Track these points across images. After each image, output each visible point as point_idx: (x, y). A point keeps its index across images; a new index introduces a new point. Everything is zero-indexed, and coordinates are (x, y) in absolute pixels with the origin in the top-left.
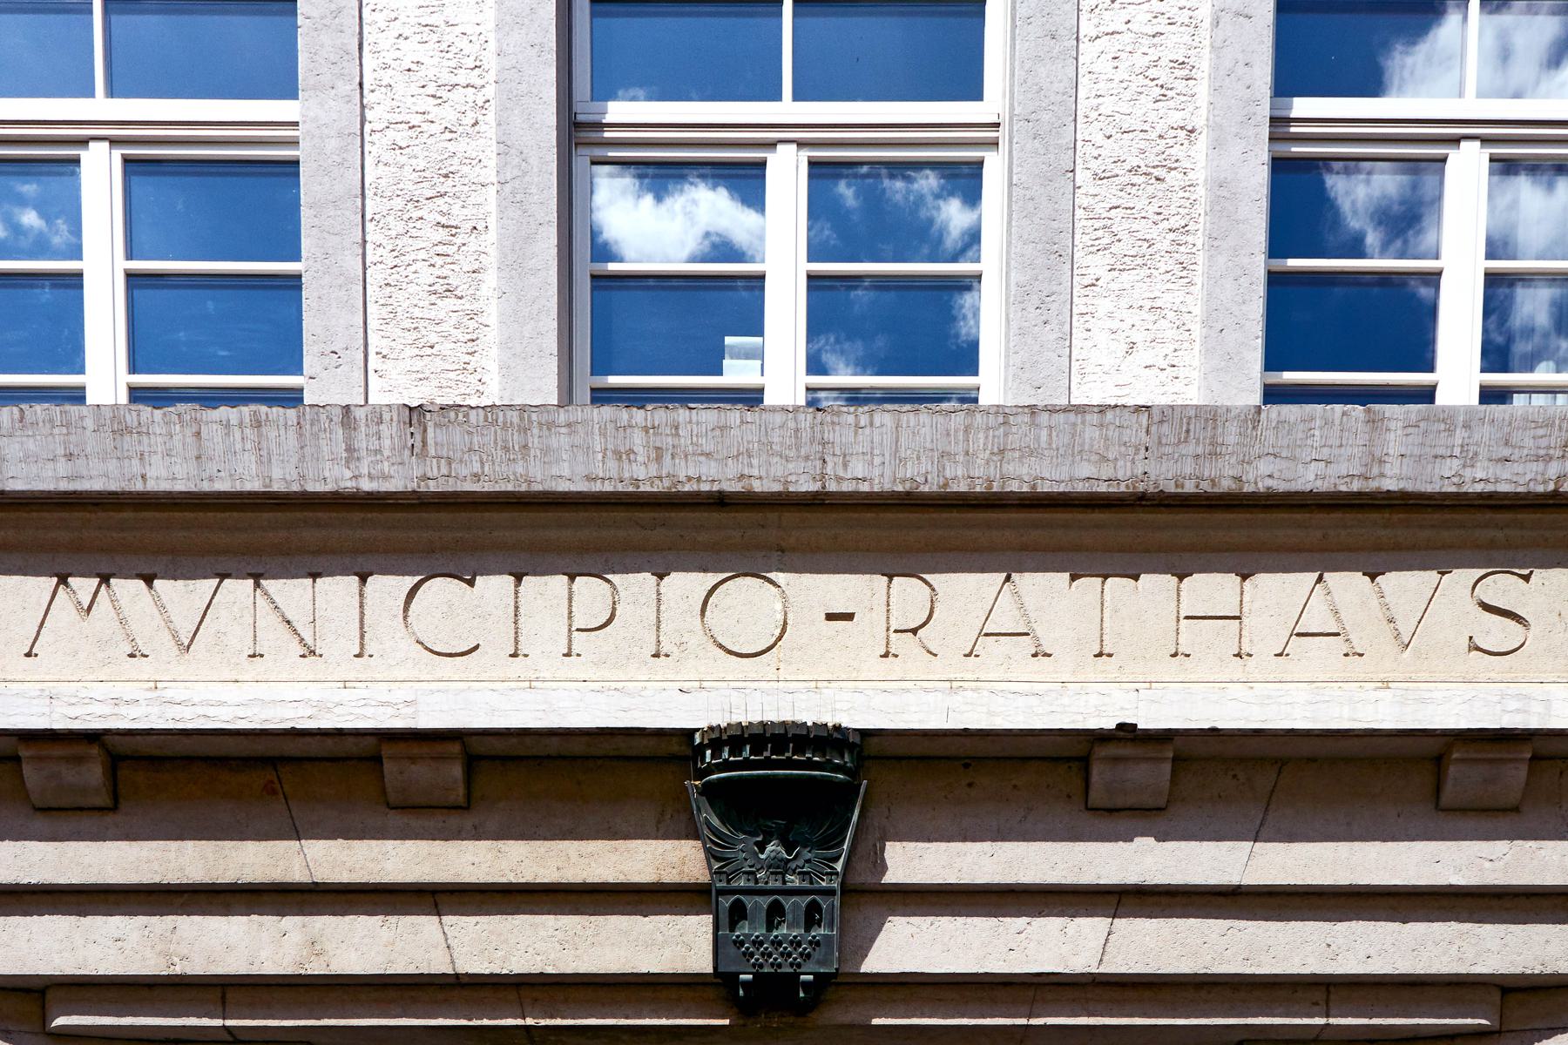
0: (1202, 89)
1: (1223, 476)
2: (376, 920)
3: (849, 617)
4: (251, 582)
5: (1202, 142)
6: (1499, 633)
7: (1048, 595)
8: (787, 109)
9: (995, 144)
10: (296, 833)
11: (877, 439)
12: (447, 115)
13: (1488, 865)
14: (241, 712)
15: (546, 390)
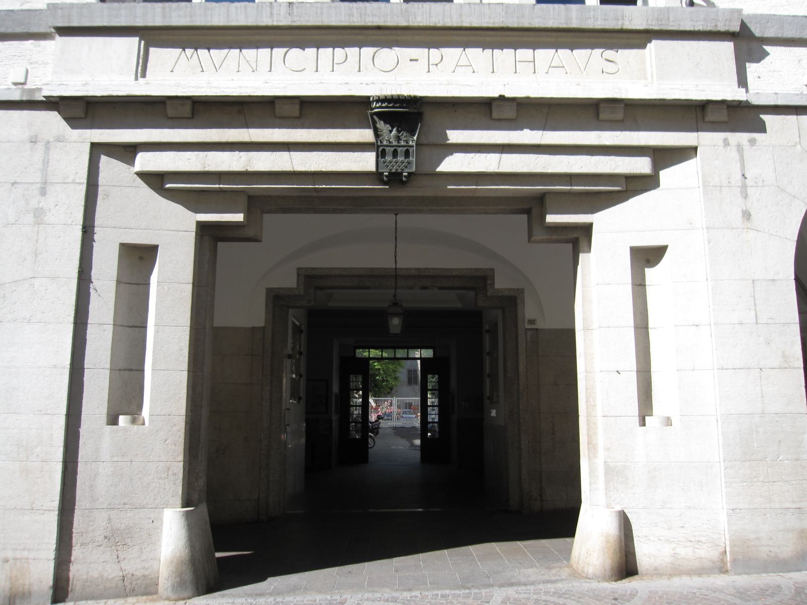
1: (526, 23)
2: (269, 153)
3: (417, 60)
6: (610, 67)
11: (424, 12)
13: (615, 138)
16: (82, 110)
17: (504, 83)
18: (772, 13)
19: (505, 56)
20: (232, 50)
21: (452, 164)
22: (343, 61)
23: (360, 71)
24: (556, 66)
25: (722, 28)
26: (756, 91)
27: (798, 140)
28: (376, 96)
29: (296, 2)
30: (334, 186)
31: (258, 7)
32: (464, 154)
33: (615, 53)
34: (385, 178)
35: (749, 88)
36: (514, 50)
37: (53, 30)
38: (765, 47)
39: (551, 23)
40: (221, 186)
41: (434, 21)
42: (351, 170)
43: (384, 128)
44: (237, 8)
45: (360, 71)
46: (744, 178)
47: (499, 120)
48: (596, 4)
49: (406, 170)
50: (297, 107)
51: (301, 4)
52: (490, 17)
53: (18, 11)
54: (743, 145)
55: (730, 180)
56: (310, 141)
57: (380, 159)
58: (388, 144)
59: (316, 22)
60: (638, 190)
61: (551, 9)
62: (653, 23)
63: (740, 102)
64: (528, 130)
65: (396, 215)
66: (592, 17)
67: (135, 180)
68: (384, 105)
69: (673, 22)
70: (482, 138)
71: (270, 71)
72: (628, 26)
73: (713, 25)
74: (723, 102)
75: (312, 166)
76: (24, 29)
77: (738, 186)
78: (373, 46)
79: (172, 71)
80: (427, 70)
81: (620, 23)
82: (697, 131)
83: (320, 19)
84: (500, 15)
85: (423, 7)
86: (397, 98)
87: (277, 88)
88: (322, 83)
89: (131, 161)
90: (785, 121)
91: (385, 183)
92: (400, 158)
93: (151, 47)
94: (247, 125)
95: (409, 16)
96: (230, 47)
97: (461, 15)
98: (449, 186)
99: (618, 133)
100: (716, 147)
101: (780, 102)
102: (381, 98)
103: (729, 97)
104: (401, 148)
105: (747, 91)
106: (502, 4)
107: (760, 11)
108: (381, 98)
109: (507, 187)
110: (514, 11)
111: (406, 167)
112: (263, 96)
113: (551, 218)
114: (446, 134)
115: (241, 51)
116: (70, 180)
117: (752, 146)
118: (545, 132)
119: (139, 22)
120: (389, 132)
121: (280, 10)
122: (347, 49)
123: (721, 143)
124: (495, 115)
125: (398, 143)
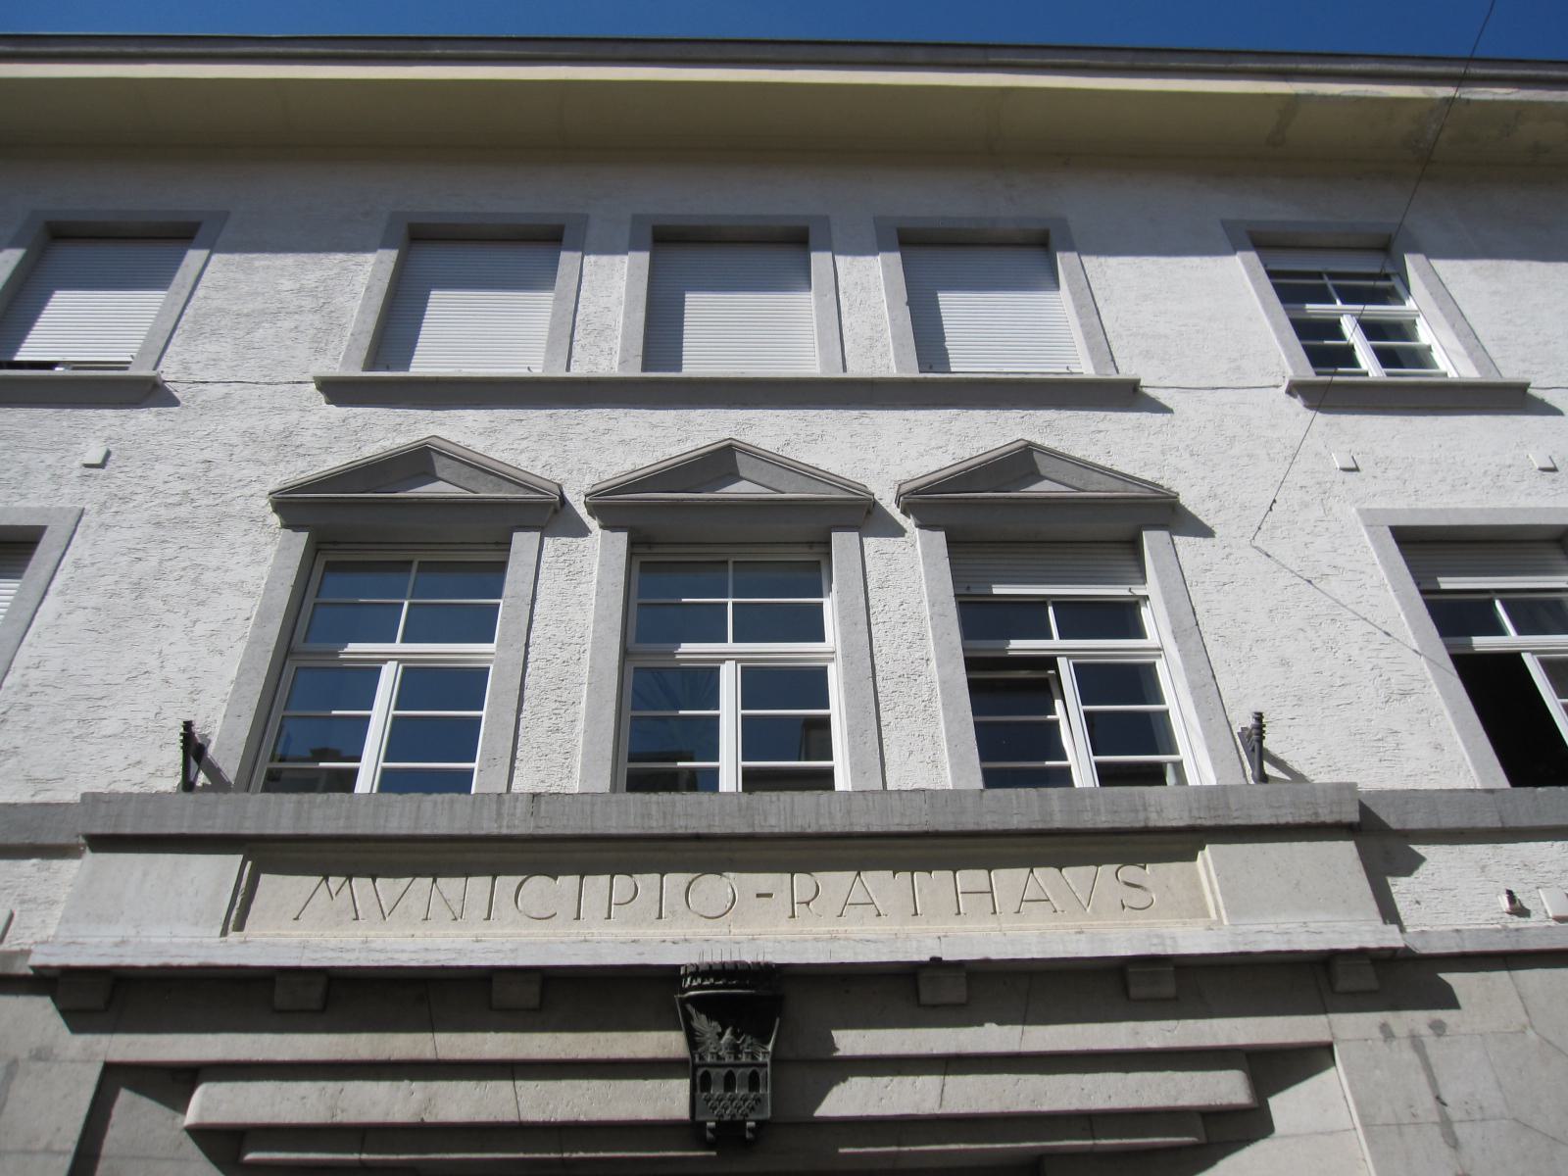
1: (969, 823)
2: (473, 1084)
3: (770, 895)
4: (431, 879)
5: (933, 664)
6: (1136, 898)
7: (879, 883)
8: (730, 646)
11: (782, 807)
12: (565, 655)
13: (1168, 1034)
14: (413, 956)
15: (603, 784)
16: (97, 995)
17: (939, 934)
18: (1410, 786)
19: (935, 884)
20: (418, 879)
22: (629, 899)
24: (1034, 898)
25: (1327, 817)
26: (1419, 929)
27: (1524, 1019)
28: (692, 965)
29: (546, 792)
30: (602, 1154)
31: (474, 803)
33: (1141, 870)
34: (709, 1135)
35: (1405, 924)
36: (951, 873)
37: (82, 841)
38: (1415, 847)
39: (1015, 822)
40: (364, 1156)
41: (800, 824)
42: (638, 1118)
43: (708, 1030)
46: (1440, 1105)
47: (934, 1006)
49: (751, 1117)
51: (555, 797)
52: (903, 815)
53: (25, 805)
54: (1421, 1036)
55: (1413, 1110)
56: (558, 1057)
57: (699, 1092)
58: (715, 1060)
59: (581, 828)
61: (1014, 797)
63: (1394, 950)
64: (994, 1025)
66: (1089, 808)
67: (181, 1144)
68: (706, 983)
69: (1236, 810)
70: (903, 1044)
71: (489, 918)
72: (1156, 821)
73: (1310, 812)
75: (559, 1111)
76: (28, 838)
77: (1434, 1123)
78: (687, 871)
79: (297, 919)
80: (790, 914)
81: (1141, 816)
82: (1325, 1012)
83: (589, 823)
84: (921, 810)
85: (779, 799)
86: (733, 968)
87: (498, 951)
88: (586, 941)
89: (180, 1104)
90: (1489, 983)
91: (709, 1146)
92: (740, 1092)
93: (264, 873)
94: (432, 1026)
96: (415, 875)
97: (849, 812)
98: (843, 1147)
99: (1172, 1023)
100: (1370, 1042)
101: (1470, 947)
102: (701, 968)
103: (1371, 941)
104: (741, 1070)
105: (1402, 930)
107: (1389, 784)
108: (701, 968)
110: (946, 801)
111: (752, 1109)
112: (470, 968)
115: (435, 881)
116: (41, 1144)
117: (1439, 1035)
118: (1026, 1028)
119: (249, 828)
120: (717, 1037)
121: (515, 808)
122: (637, 877)
123: (1377, 1034)
124: (926, 996)
125: (736, 1058)
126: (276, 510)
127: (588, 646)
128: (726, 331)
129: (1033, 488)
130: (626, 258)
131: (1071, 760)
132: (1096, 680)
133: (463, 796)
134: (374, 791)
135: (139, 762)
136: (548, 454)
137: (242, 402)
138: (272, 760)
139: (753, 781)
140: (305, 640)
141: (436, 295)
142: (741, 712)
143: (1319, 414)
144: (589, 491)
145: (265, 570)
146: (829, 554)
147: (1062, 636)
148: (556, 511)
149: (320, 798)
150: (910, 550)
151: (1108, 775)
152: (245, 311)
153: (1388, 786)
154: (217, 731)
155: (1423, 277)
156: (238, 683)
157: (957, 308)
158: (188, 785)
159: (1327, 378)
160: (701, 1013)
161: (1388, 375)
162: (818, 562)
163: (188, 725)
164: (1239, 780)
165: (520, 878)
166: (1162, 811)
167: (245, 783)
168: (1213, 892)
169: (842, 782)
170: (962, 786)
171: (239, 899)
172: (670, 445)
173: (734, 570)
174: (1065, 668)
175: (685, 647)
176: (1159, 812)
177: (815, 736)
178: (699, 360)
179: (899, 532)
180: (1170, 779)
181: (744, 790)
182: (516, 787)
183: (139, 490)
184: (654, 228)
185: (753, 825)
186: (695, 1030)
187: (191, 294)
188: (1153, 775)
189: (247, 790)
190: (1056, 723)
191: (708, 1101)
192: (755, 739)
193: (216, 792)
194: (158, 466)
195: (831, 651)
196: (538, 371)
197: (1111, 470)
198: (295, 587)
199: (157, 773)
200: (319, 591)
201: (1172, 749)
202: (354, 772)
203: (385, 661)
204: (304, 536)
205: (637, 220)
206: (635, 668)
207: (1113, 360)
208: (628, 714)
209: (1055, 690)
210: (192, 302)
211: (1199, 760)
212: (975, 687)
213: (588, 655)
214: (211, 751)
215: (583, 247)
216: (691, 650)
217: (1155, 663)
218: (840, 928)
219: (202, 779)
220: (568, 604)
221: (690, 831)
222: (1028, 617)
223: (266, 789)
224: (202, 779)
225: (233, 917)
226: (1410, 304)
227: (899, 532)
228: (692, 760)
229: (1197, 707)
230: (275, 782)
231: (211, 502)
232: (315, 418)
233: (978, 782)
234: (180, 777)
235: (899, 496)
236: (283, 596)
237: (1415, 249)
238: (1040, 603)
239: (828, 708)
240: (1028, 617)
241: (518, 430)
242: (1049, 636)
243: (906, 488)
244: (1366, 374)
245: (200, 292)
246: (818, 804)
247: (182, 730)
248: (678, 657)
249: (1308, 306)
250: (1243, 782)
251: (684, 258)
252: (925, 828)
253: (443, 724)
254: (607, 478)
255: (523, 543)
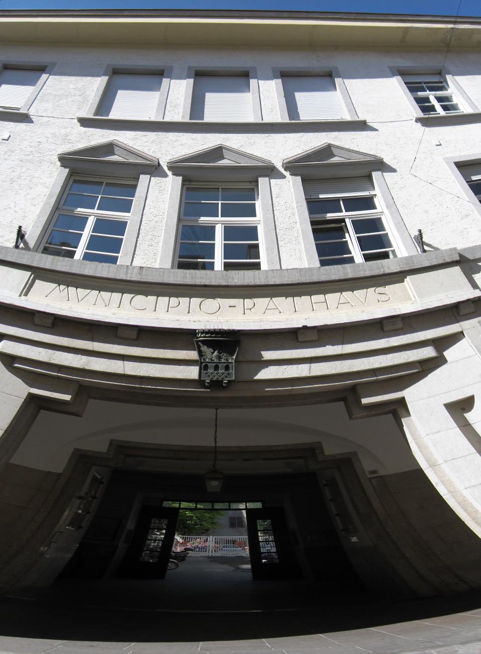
0: (297, 216)
1: (315, 279)
5: (298, 224)
6: (383, 298)
7: (279, 301)
8: (220, 218)
9: (259, 223)
10: (93, 340)
14: (88, 316)
15: (168, 265)
21: (265, 374)
22: (177, 304)
23: (189, 313)
25: (448, 260)
30: (158, 387)
31: (118, 267)
32: (278, 367)
34: (206, 384)
40: (59, 374)
44: (103, 266)
45: (189, 313)
48: (362, 262)
50: (136, 333)
52: (289, 278)
57: (203, 371)
60: (431, 368)
62: (404, 267)
65: (217, 409)
69: (417, 263)
72: (387, 271)
74: (468, 300)
79: (47, 296)
80: (243, 313)
81: (382, 270)
83: (162, 279)
85: (238, 273)
87: (121, 319)
88: (157, 319)
94: (92, 339)
95: (228, 279)
96: (92, 289)
97: (267, 277)
104: (221, 364)
106: (297, 269)
109: (320, 385)
111: (227, 377)
113: (365, 401)
114: (261, 354)
115: (100, 292)
118: (343, 346)
119: (35, 264)
121: (133, 271)
122: (180, 299)
125: (219, 360)
126: (59, 161)
127: (165, 217)
128: (221, 106)
129: (332, 160)
130: (185, 81)
131: (353, 254)
132: (359, 225)
133: (113, 265)
134: (81, 259)
135: (2, 236)
136: (154, 148)
137: (53, 124)
138: (46, 243)
139: (227, 267)
140: (63, 205)
141: (120, 92)
142: (223, 260)
143: (426, 128)
144: (169, 161)
145: (53, 180)
146: (257, 186)
147: (346, 211)
148: (156, 168)
149: (61, 258)
150: (287, 183)
151: (368, 258)
152: (58, 94)
153: (467, 246)
154: (29, 231)
155: (452, 82)
156: (39, 216)
157: (301, 97)
158: (17, 247)
159: (427, 116)
160: (205, 345)
161: (446, 113)
162: (254, 188)
163: (20, 227)
164: (416, 253)
165: (133, 295)
166: (389, 267)
167: (36, 249)
168: (412, 292)
169: (264, 267)
170: (312, 266)
171: (27, 286)
172: (199, 146)
173: (222, 191)
174: (348, 223)
175: (202, 218)
176: (389, 268)
177: (253, 251)
178: (210, 116)
179: (284, 177)
180: (391, 256)
181: (224, 270)
182: (134, 264)
183: (17, 149)
184: (195, 71)
185: (228, 282)
186: (202, 351)
187: (42, 88)
188: (385, 256)
189: (36, 252)
190: (346, 242)
191: (207, 374)
192: (228, 251)
193: (26, 250)
194: (24, 142)
195: (260, 220)
196: (153, 119)
197: (359, 152)
198: (62, 187)
199: (8, 241)
200: (70, 189)
201: (391, 246)
202: (75, 252)
203: (90, 215)
204: (67, 170)
205: (189, 68)
206: (183, 225)
207: (357, 114)
208: (179, 241)
209: (345, 230)
210: (42, 90)
211: (402, 249)
212: (315, 231)
213: (165, 219)
214: (26, 237)
215: (170, 77)
216: (204, 220)
217: (381, 218)
218: (264, 317)
219: (22, 245)
220: (158, 205)
221: (202, 284)
222: (333, 205)
223: (43, 252)
224: (22, 245)
225: (24, 291)
226: (449, 91)
227: (284, 177)
228: (204, 259)
229: (398, 230)
230: (46, 251)
231: (39, 155)
232: (76, 131)
233: (318, 264)
234: (14, 244)
235: (283, 164)
236: (58, 190)
237: (449, 74)
238: (337, 200)
239: (259, 259)
240: (333, 205)
241: (145, 139)
242: (342, 211)
243: (285, 161)
244: (439, 114)
245: (44, 88)
246: (254, 274)
247: (18, 228)
248: (199, 222)
249: (419, 93)
250: (418, 253)
251: (204, 81)
252: (298, 282)
253: (108, 240)
254: (175, 157)
255: (144, 179)
